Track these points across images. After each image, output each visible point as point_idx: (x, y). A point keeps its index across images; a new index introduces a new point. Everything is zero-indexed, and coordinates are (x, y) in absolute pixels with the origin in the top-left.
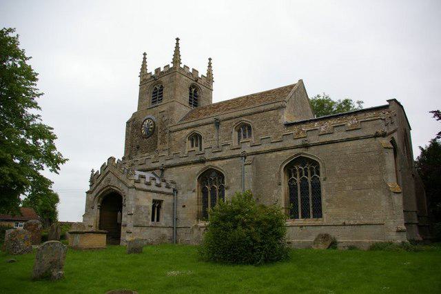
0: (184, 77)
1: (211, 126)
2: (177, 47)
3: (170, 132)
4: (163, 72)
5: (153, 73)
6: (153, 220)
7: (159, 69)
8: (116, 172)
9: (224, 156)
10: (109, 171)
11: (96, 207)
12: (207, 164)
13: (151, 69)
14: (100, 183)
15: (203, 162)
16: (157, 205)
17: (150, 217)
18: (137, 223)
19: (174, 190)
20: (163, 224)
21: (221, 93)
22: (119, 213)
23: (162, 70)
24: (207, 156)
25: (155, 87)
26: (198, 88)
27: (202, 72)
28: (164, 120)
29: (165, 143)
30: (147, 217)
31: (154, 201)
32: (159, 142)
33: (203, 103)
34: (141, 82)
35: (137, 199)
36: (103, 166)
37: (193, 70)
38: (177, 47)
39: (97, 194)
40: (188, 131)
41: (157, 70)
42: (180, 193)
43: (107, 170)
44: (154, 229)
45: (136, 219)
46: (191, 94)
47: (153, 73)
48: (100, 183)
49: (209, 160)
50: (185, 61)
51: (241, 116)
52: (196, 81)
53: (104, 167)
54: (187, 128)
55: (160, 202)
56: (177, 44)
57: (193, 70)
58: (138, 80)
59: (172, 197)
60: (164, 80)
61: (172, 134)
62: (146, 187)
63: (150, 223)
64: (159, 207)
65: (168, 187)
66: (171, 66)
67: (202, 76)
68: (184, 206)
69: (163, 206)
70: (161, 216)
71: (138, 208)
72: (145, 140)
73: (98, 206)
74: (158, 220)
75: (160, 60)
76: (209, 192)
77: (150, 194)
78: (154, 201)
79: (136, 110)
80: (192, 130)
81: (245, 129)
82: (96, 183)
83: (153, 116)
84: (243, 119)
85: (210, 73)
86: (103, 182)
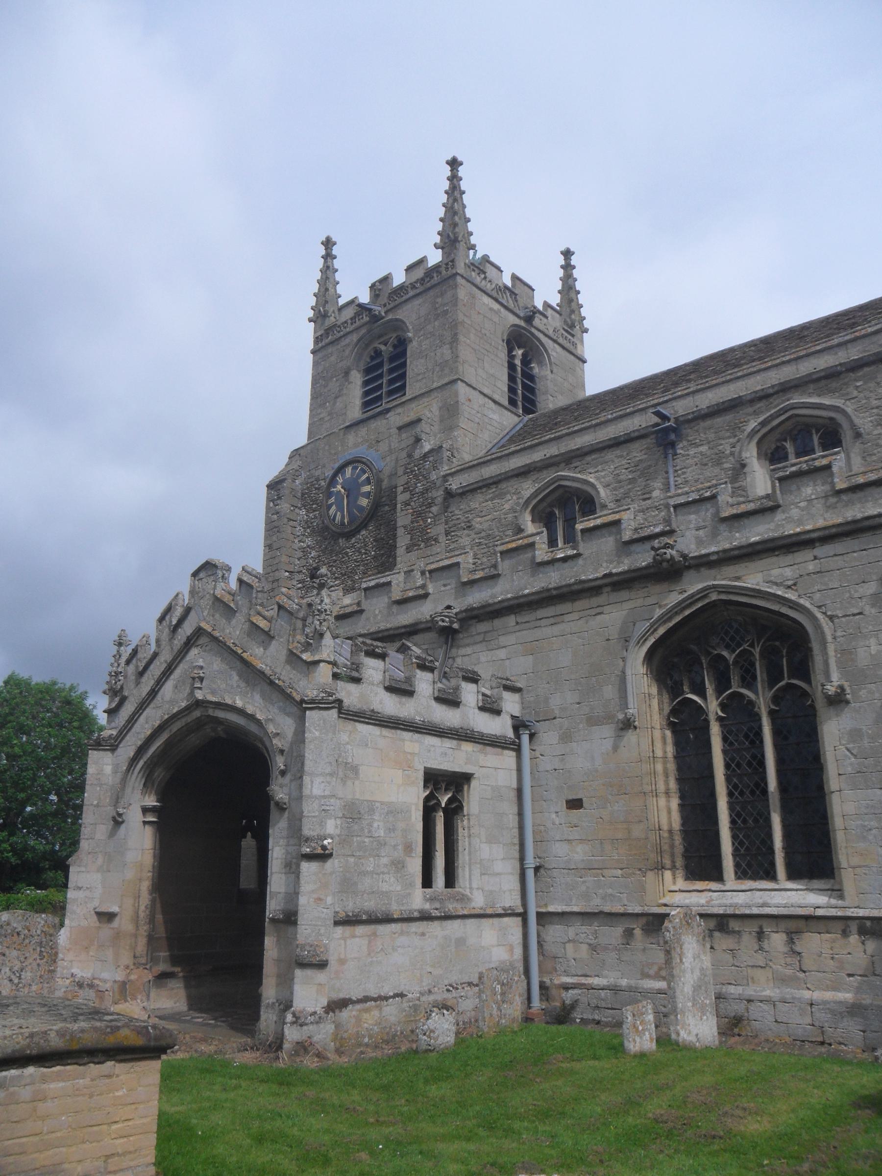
0: (486, 300)
1: (637, 452)
2: (455, 191)
3: (449, 495)
4: (402, 287)
5: (365, 298)
6: (427, 882)
7: (386, 279)
8: (233, 632)
9: (791, 530)
10: (199, 632)
11: (134, 817)
12: (694, 584)
13: (354, 288)
14: (153, 693)
15: (666, 572)
16: (445, 793)
17: (415, 865)
18: (351, 906)
19: (518, 725)
20: (478, 902)
21: (615, 355)
22: (248, 843)
23: (399, 279)
24: (691, 539)
25: (374, 347)
26: (535, 340)
27: (546, 292)
28: (417, 454)
29: (431, 541)
30: (398, 865)
31: (435, 780)
32: (403, 540)
33: (551, 400)
34: (317, 340)
35: (349, 771)
36: (169, 610)
37: (515, 278)
38: (455, 191)
39: (141, 751)
40: (528, 488)
41: (380, 287)
42: (549, 737)
43: (188, 629)
44: (435, 928)
45: (347, 885)
46: (512, 367)
47: (365, 298)
48: (153, 693)
49: (705, 563)
50: (487, 238)
51: (785, 388)
52: (529, 319)
53: (171, 618)
54: (523, 473)
55: (458, 781)
56: (454, 179)
57: (515, 278)
58: (307, 334)
59: (509, 757)
60: (410, 315)
61: (458, 510)
62: (390, 705)
63: (418, 899)
64: (454, 811)
65: (490, 708)
66: (435, 257)
67: (547, 305)
68: (575, 804)
69: (474, 799)
70: (463, 858)
71: (353, 814)
72: (341, 541)
73: (145, 810)
74: (450, 881)
75: (390, 247)
76: (715, 730)
77: (411, 742)
78: (435, 780)
79: (302, 439)
80: (548, 476)
81: (801, 438)
82: (135, 694)
83: (380, 446)
84: (797, 399)
85: (569, 288)
86: (168, 689)
